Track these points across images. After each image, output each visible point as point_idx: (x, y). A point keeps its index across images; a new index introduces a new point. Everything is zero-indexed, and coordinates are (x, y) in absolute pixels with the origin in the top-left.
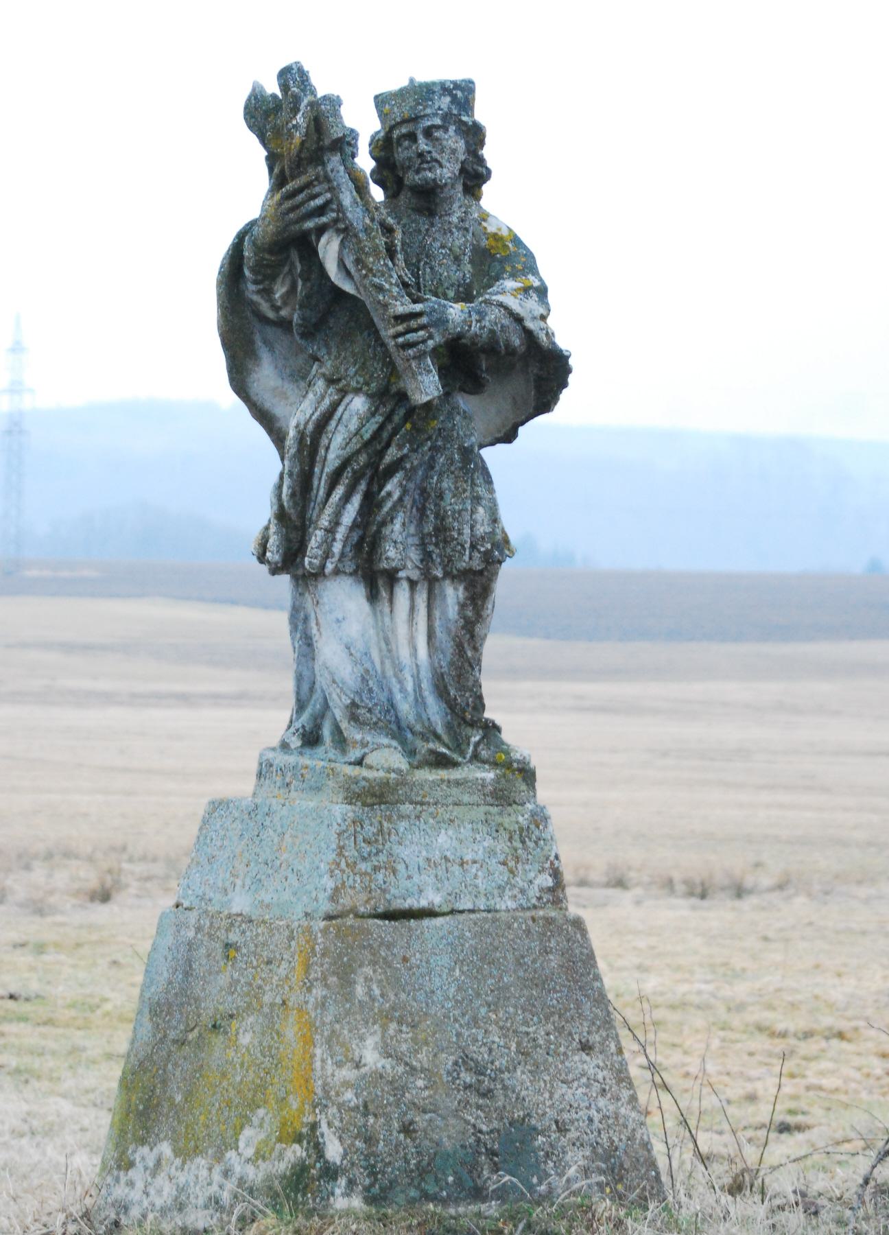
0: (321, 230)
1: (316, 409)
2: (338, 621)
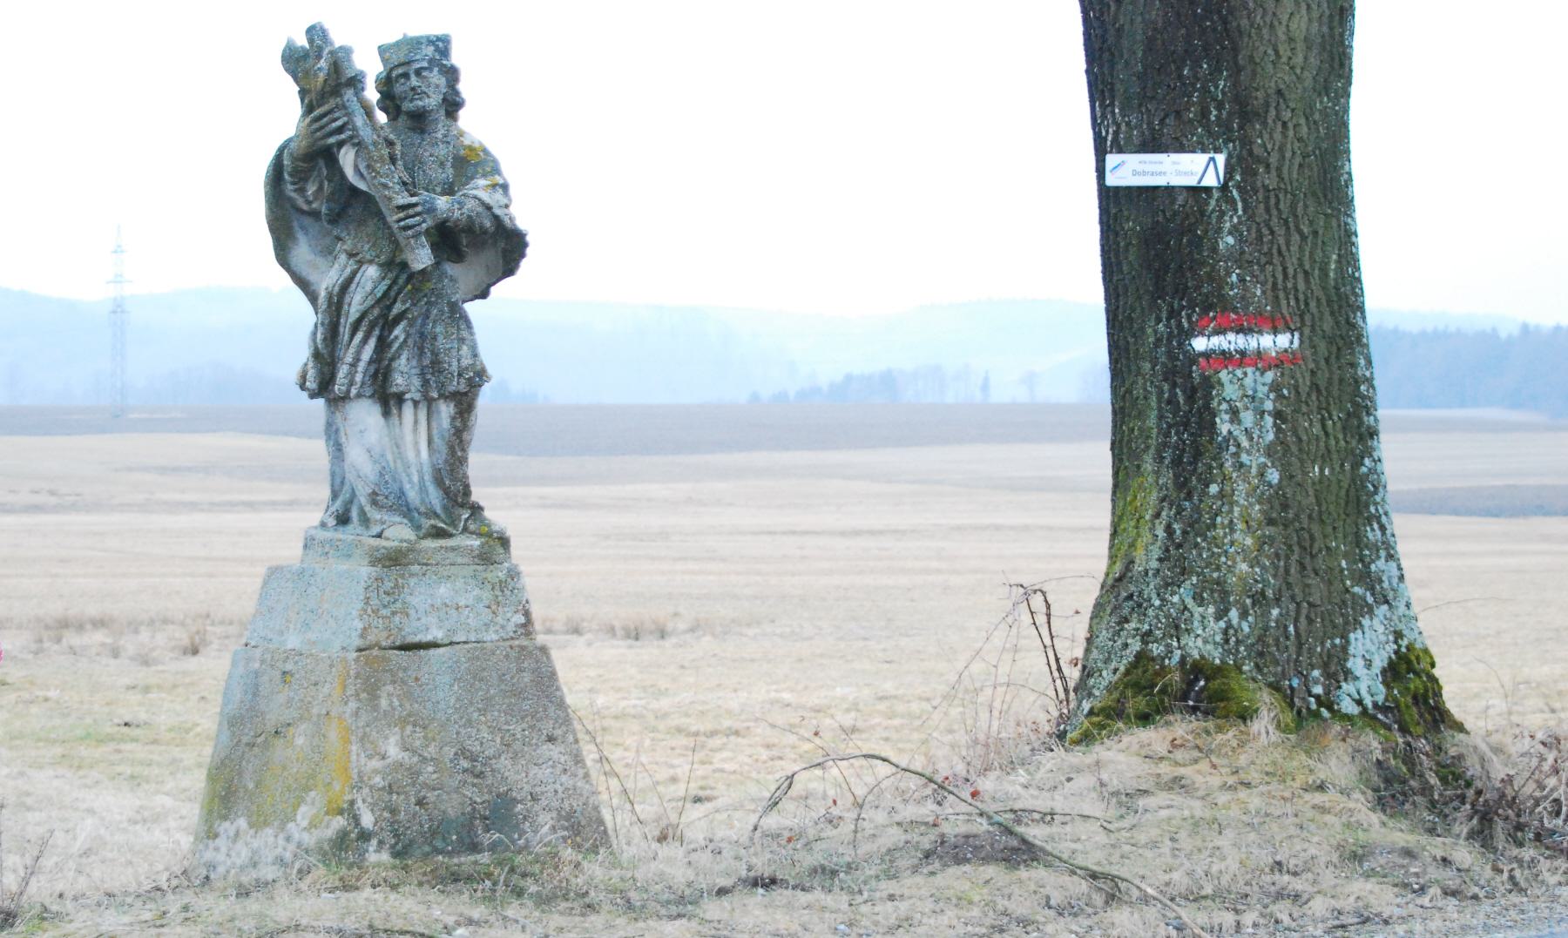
0: (341, 144)
2: (361, 432)
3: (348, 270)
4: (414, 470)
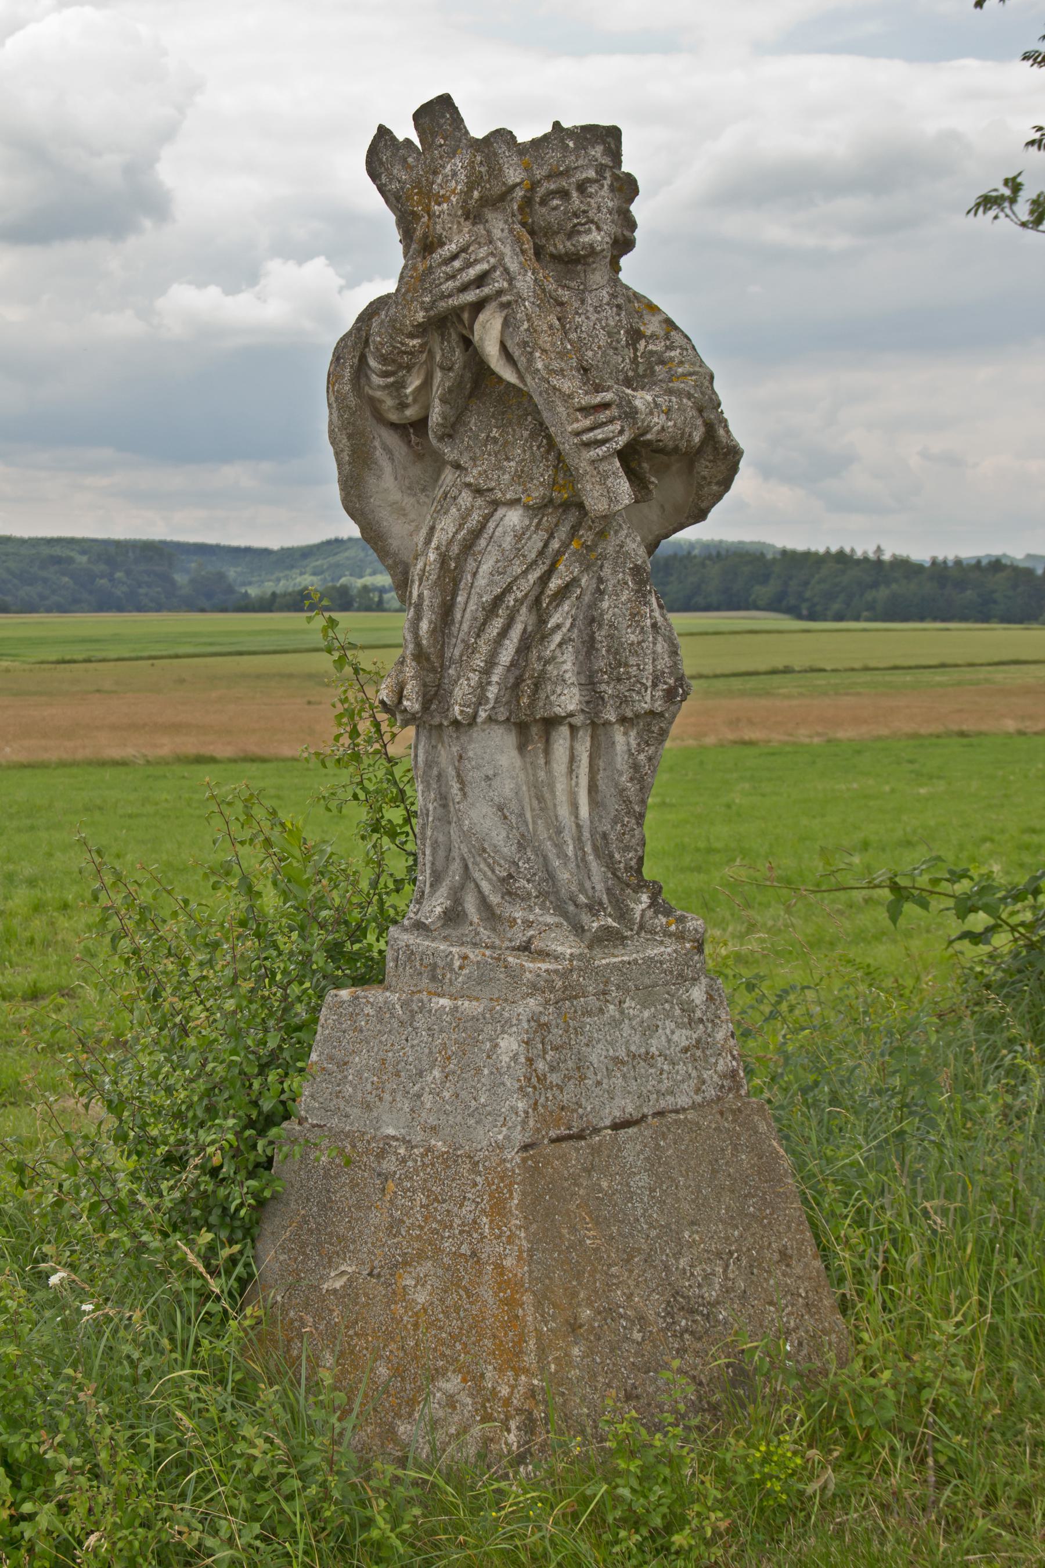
0: (478, 307)
1: (461, 526)
2: (488, 778)
3: (476, 517)
4: (568, 836)
